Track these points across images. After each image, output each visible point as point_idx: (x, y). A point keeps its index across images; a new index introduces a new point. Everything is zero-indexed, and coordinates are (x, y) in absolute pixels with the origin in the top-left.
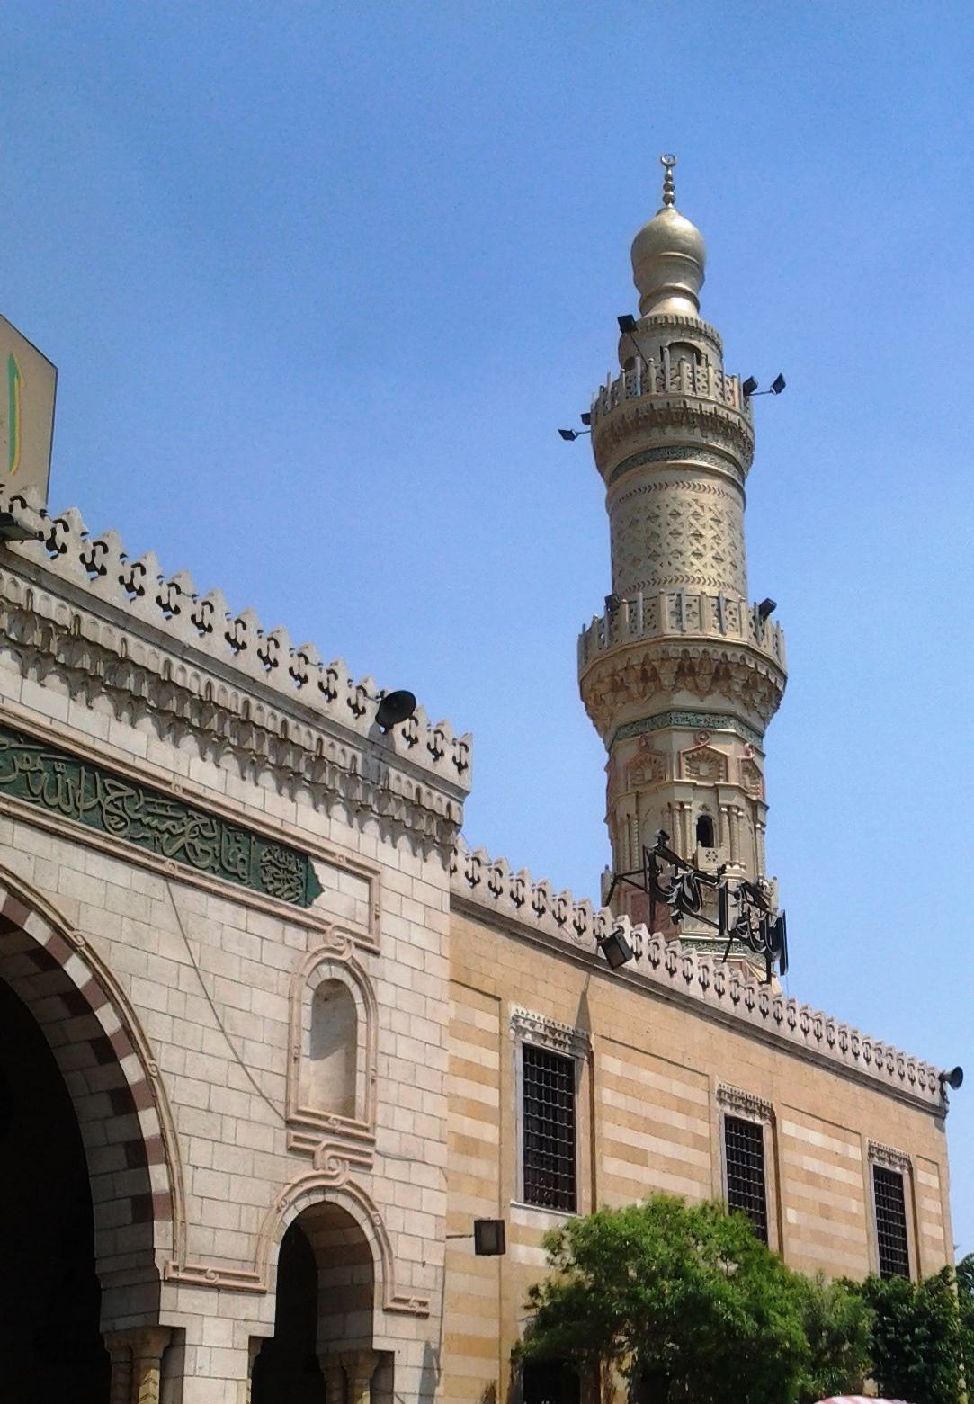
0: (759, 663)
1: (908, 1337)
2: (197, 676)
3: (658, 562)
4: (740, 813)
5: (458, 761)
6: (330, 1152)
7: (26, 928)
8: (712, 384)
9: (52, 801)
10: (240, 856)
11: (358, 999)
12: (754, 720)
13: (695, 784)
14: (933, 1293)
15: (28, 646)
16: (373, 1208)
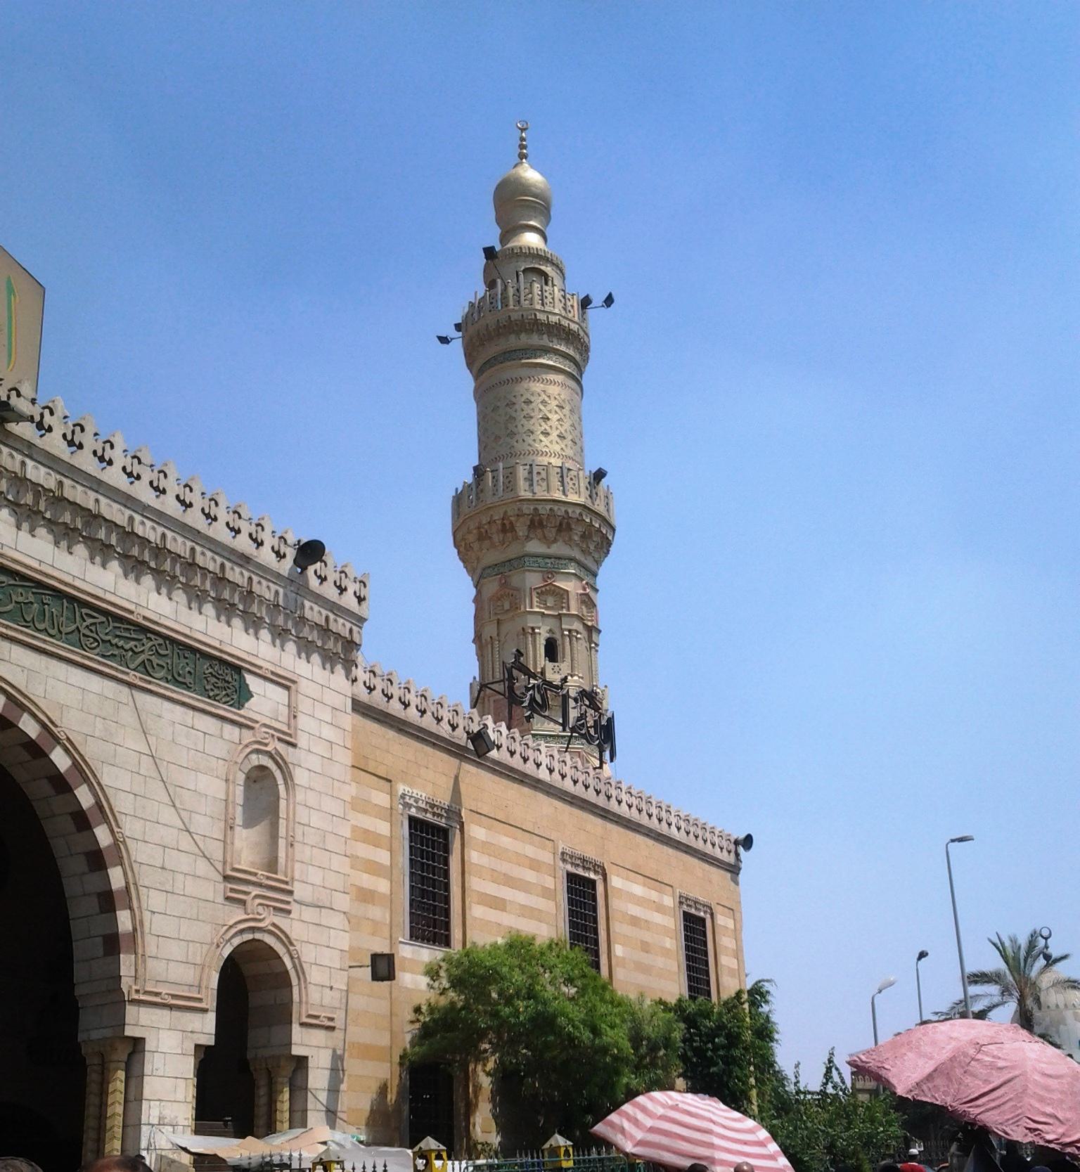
0: (593, 518)
1: (710, 1045)
2: (154, 529)
4: (579, 636)
6: (258, 901)
7: (20, 725)
8: (556, 301)
9: (41, 626)
10: (188, 669)
11: (280, 781)
12: (589, 563)
13: (543, 613)
15: (22, 505)
16: (292, 944)
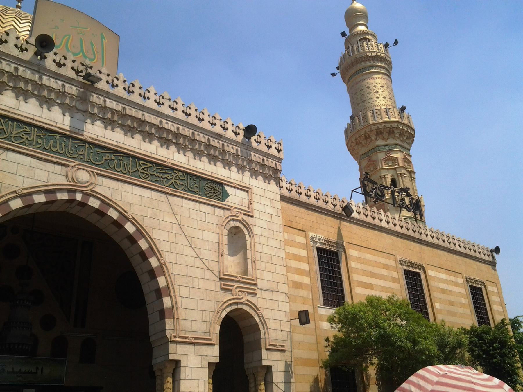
1: (491, 348)
3: (365, 103)
4: (405, 175)
5: (277, 149)
8: (374, 47)
10: (196, 185)
12: (405, 145)
13: (388, 168)
14: (499, 330)
16: (259, 310)
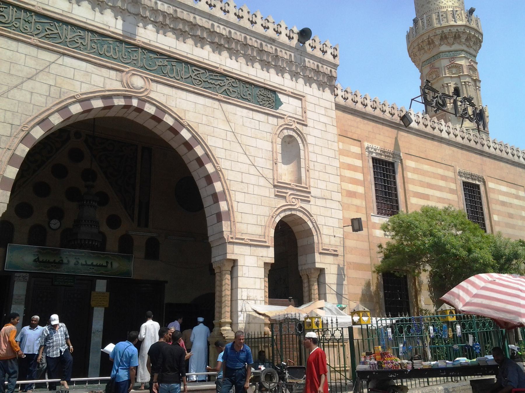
0: (471, 30)
2: (224, 29)
3: (430, 4)
10: (248, 93)
12: (472, 51)
13: (451, 76)
16: (312, 216)
